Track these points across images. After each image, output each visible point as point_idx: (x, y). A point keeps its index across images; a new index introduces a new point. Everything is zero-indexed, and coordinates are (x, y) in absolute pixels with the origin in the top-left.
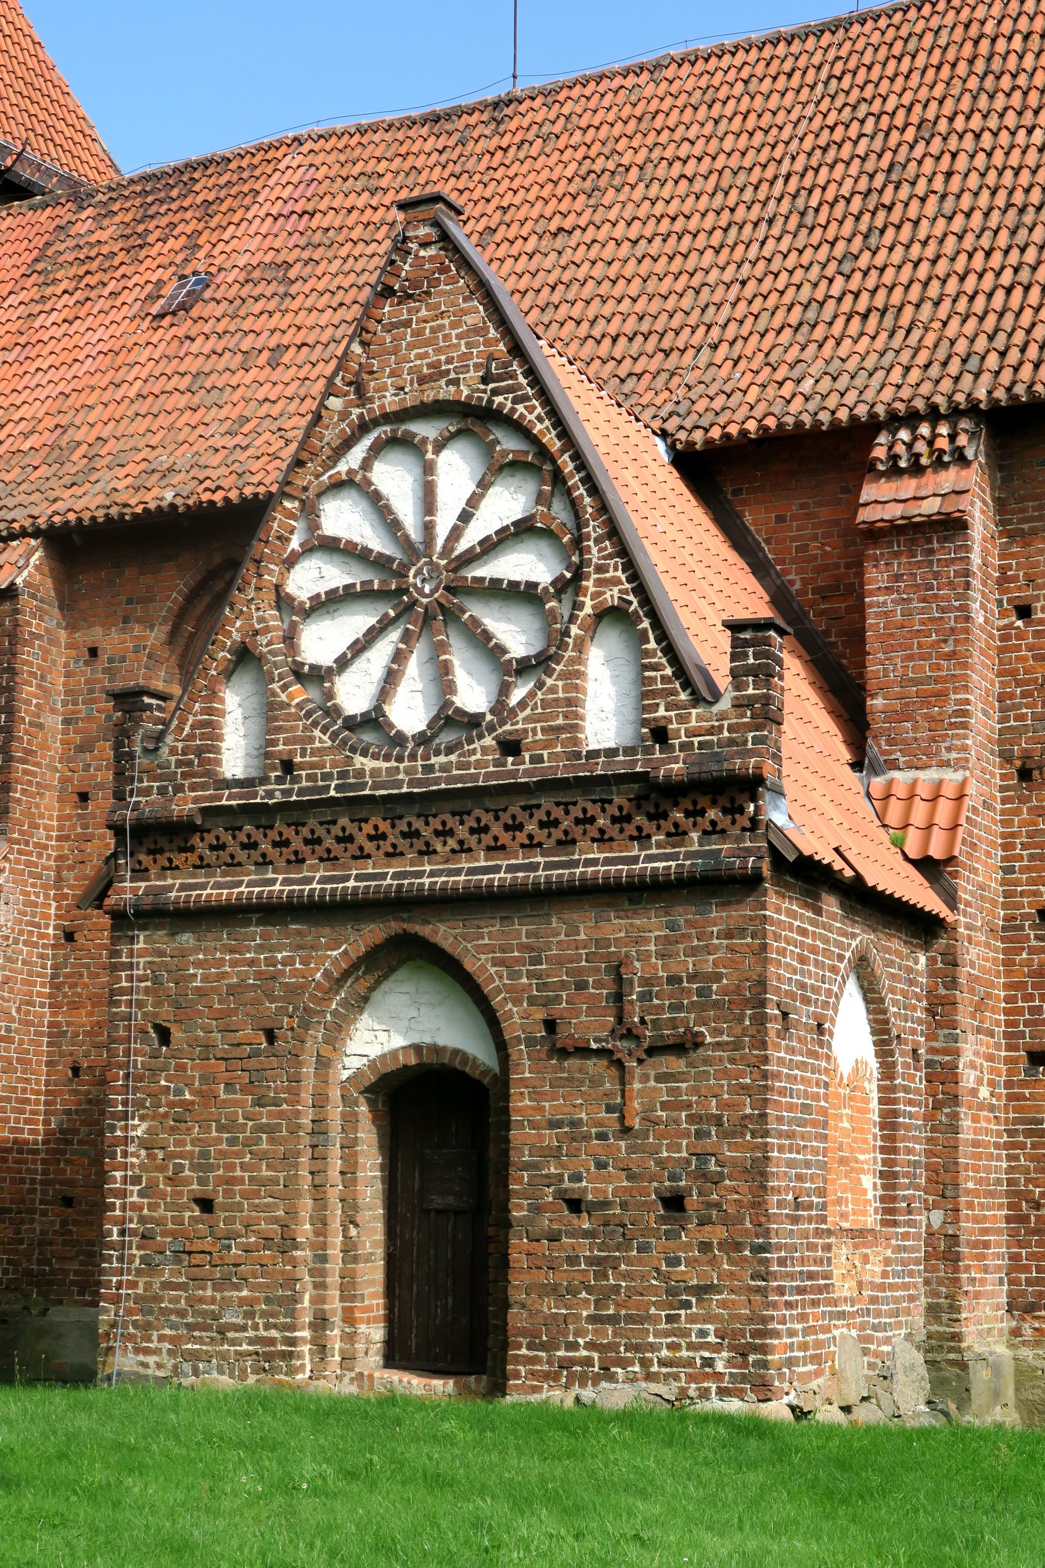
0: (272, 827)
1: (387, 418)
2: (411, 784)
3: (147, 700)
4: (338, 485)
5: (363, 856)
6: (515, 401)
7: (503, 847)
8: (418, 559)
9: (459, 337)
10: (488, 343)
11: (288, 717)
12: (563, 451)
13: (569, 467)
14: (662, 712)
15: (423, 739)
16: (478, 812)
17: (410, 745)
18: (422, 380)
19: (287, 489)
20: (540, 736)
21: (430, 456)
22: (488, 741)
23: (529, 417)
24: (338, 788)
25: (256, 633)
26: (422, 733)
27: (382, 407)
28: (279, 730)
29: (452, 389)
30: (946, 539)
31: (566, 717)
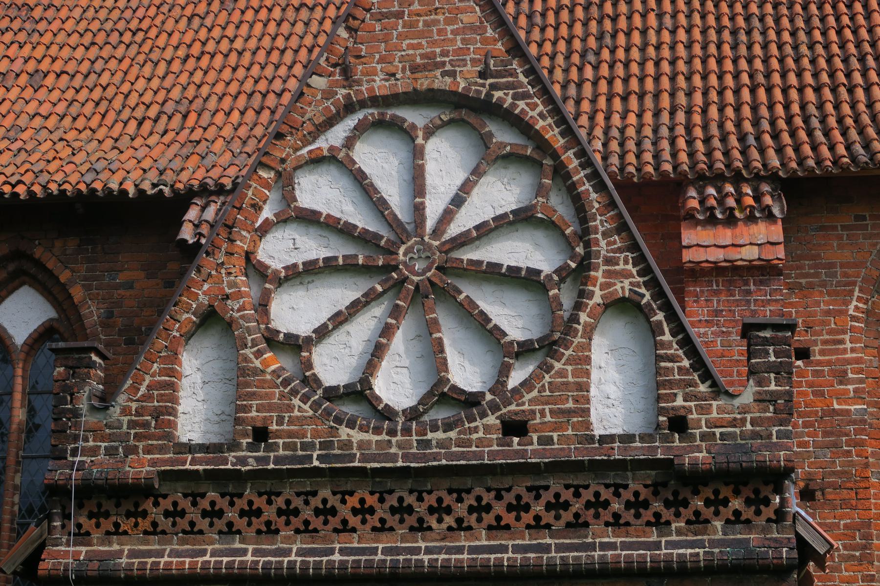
0: (240, 496)
1: (374, 101)
2: (405, 457)
3: (94, 358)
4: (317, 161)
5: (345, 528)
6: (516, 97)
7: (507, 527)
8: (409, 237)
9: (455, 32)
10: (485, 41)
11: (262, 384)
12: (566, 149)
13: (573, 163)
14: (679, 402)
15: (413, 414)
16: (479, 490)
17: (401, 420)
18: (415, 69)
19: (264, 159)
20: (548, 418)
21: (420, 141)
22: (492, 420)
23: (531, 113)
24: (319, 458)
25: (227, 297)
26: (413, 409)
27: (371, 90)
28: (252, 396)
29: (448, 80)
30: (762, 283)
31: (576, 401)
